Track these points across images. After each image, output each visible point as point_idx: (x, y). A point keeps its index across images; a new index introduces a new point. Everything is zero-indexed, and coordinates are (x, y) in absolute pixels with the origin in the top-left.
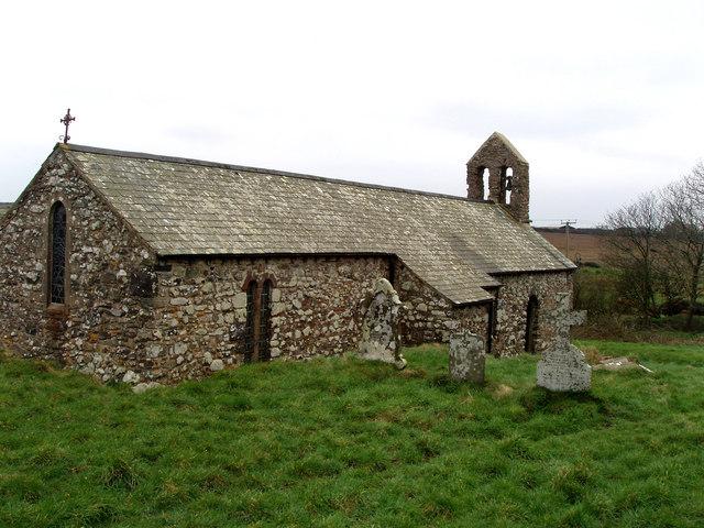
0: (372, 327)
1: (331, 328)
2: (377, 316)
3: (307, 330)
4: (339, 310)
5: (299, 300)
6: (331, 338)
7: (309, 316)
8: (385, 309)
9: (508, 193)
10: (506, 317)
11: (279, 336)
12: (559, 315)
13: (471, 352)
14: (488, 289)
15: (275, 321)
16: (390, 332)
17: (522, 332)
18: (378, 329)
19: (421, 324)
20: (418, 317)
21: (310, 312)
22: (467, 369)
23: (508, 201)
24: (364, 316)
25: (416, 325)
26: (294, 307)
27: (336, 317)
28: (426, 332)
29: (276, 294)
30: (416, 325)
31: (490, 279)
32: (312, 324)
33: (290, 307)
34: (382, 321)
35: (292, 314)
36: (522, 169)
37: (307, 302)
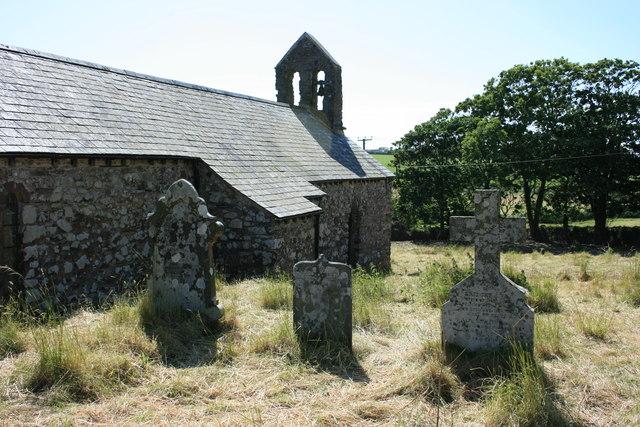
0: (168, 256)
1: (117, 255)
2: (173, 240)
3: (82, 261)
4: (126, 231)
5: (68, 220)
6: (118, 270)
7: (85, 241)
8: (187, 227)
9: (320, 99)
10: (328, 232)
11: (37, 272)
12: (480, 225)
13: (329, 291)
14: (311, 198)
15: (31, 251)
16: (195, 263)
17: (344, 247)
18: (176, 258)
19: (235, 245)
20: (231, 236)
21: (85, 235)
22: (323, 318)
23: (320, 107)
24: (155, 240)
25: (229, 246)
26: (60, 231)
27: (125, 240)
28: (242, 254)
29: (29, 213)
30: (229, 246)
31: (314, 188)
32: (89, 252)
33: (53, 230)
34: (182, 246)
35: (57, 239)
36: (334, 72)
37: (79, 223)
